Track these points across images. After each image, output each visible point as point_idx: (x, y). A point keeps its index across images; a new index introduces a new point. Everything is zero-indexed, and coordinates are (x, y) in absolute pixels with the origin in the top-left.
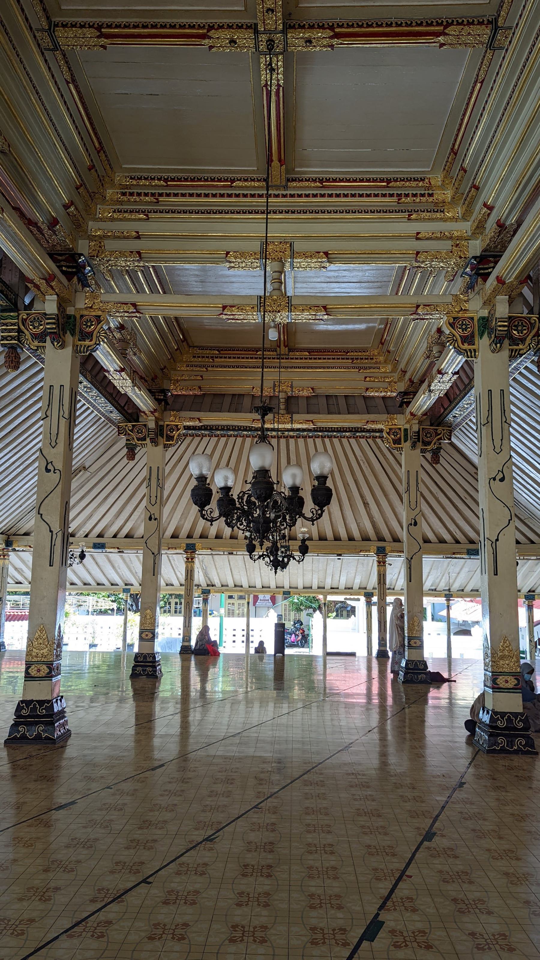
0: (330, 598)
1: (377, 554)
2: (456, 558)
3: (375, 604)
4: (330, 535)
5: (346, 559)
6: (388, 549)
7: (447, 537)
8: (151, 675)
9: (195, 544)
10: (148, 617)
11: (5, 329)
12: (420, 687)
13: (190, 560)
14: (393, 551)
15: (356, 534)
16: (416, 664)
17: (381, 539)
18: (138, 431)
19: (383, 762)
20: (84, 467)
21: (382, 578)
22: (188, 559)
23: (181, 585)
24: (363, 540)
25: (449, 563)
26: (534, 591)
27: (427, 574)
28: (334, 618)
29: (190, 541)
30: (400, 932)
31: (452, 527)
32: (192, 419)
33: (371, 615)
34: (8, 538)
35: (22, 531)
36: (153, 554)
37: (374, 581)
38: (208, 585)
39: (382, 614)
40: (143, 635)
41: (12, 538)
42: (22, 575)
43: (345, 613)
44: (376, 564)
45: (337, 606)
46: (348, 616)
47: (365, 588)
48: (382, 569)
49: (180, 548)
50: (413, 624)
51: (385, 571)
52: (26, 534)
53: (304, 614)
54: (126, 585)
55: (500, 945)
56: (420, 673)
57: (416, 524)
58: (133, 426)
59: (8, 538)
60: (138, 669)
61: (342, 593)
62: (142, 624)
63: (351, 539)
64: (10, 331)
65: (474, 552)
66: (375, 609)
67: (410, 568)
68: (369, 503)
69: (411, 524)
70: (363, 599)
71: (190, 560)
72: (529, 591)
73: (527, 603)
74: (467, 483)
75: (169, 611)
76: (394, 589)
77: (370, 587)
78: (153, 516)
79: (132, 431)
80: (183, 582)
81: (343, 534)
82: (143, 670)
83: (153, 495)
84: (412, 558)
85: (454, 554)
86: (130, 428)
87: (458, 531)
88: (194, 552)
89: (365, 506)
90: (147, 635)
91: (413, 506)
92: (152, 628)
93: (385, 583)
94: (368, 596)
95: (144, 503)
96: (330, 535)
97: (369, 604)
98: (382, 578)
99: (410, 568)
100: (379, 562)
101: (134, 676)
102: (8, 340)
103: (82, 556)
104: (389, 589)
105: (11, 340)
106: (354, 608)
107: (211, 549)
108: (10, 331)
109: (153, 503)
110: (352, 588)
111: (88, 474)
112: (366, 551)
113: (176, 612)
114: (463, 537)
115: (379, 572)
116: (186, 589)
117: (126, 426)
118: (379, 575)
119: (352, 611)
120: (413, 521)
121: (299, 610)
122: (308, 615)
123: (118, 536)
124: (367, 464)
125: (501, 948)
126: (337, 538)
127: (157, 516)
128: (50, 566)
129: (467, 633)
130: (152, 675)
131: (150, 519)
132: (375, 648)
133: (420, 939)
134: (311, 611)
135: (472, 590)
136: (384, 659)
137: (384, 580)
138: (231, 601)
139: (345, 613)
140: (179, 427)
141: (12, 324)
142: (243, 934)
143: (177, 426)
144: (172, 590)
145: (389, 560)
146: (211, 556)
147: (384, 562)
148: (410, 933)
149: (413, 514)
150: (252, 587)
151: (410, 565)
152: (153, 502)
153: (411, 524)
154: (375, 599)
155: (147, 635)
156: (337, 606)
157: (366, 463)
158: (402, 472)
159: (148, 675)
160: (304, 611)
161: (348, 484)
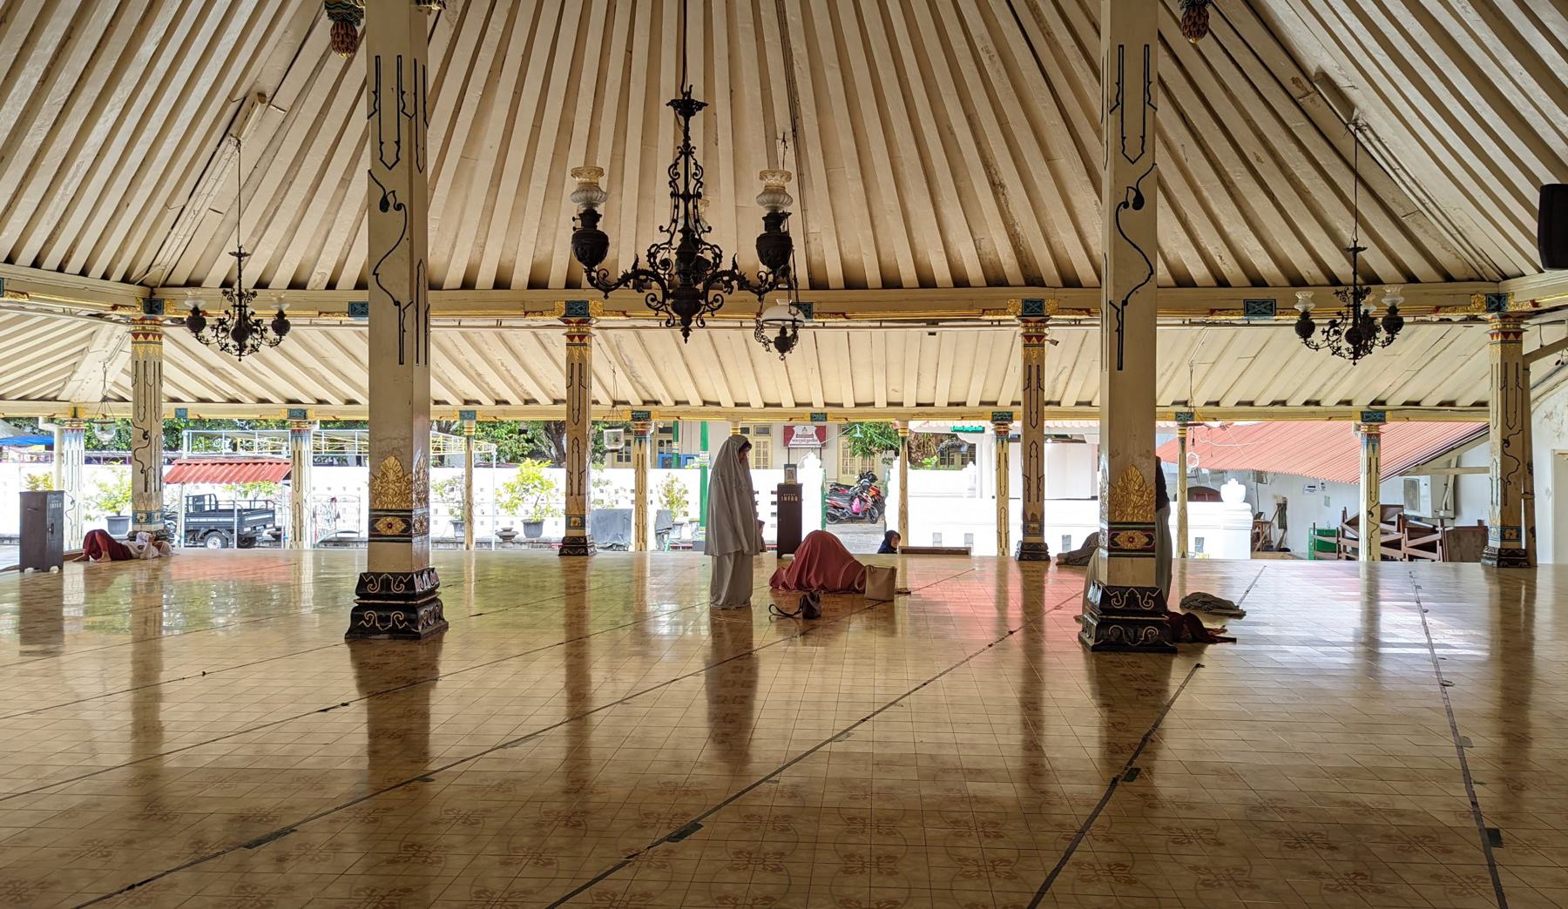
0: (914, 425)
1: (1024, 317)
2: (1214, 324)
3: (1016, 439)
4: (908, 274)
5: (947, 333)
6: (1049, 306)
7: (1198, 271)
8: (403, 631)
9: (586, 303)
10: (392, 477)
12: (1147, 662)
13: (578, 341)
14: (1062, 310)
15: (974, 271)
16: (1132, 599)
17: (1033, 279)
19: (1034, 765)
20: (261, 95)
21: (1033, 377)
22: (571, 337)
23: (556, 402)
24: (989, 284)
25: (1194, 340)
26: (1383, 403)
28: (936, 467)
29: (574, 295)
31: (1215, 247)
33: (1000, 540)
34: (152, 294)
35: (181, 276)
36: (397, 303)
37: (1010, 390)
38: (645, 403)
39: (1034, 460)
40: (380, 526)
41: (161, 293)
42: (232, 383)
43: (957, 458)
44: (1019, 342)
45: (942, 445)
46: (964, 463)
47: (995, 403)
48: (1035, 352)
49: (552, 311)
50: (1125, 488)
51: (1041, 357)
53: (878, 458)
54: (467, 402)
56: (1145, 624)
57: (1139, 202)
59: (152, 294)
60: (367, 614)
61: (942, 415)
62: (375, 495)
63: (960, 281)
65: (1262, 308)
66: (1015, 452)
67: (1120, 331)
68: (1006, 181)
69: (1126, 205)
70: (989, 426)
71: (578, 341)
72: (1372, 403)
73: (1364, 428)
74: (1267, 113)
76: (1059, 404)
77: (1004, 403)
78: (390, 198)
80: (563, 394)
81: (942, 273)
82: (381, 619)
83: (390, 138)
84: (1125, 303)
85: (1212, 312)
87: (1226, 253)
89: (995, 193)
90: (390, 526)
91: (1133, 151)
92: (404, 506)
93: (1040, 387)
94: (1001, 419)
95: (365, 163)
96: (908, 274)
97: (1002, 437)
98: (1033, 377)
99: (1120, 331)
100: (1027, 337)
101: (357, 634)
103: (281, 326)
104: (1048, 403)
106: (972, 447)
107: (624, 313)
109: (390, 160)
110: (964, 404)
111: (276, 116)
112: (997, 311)
114: (1238, 270)
115: (1027, 359)
116: (571, 409)
119: (970, 455)
120: (1132, 194)
121: (867, 453)
122: (884, 461)
124: (999, 65)
126: (926, 282)
127: (402, 198)
129: (1214, 496)
130: (406, 631)
131: (384, 205)
132: (1016, 536)
134: (891, 453)
135: (1238, 404)
136: (1038, 565)
137: (1040, 379)
139: (957, 458)
145: (1052, 332)
146: (631, 332)
147: (1041, 337)
149: (1132, 175)
150: (958, 404)
151: (1121, 323)
153: (1126, 205)
154: (1016, 427)
155: (390, 526)
156: (942, 445)
157: (997, 58)
158: (1103, 49)
159: (395, 633)
160: (878, 455)
161: (950, 128)
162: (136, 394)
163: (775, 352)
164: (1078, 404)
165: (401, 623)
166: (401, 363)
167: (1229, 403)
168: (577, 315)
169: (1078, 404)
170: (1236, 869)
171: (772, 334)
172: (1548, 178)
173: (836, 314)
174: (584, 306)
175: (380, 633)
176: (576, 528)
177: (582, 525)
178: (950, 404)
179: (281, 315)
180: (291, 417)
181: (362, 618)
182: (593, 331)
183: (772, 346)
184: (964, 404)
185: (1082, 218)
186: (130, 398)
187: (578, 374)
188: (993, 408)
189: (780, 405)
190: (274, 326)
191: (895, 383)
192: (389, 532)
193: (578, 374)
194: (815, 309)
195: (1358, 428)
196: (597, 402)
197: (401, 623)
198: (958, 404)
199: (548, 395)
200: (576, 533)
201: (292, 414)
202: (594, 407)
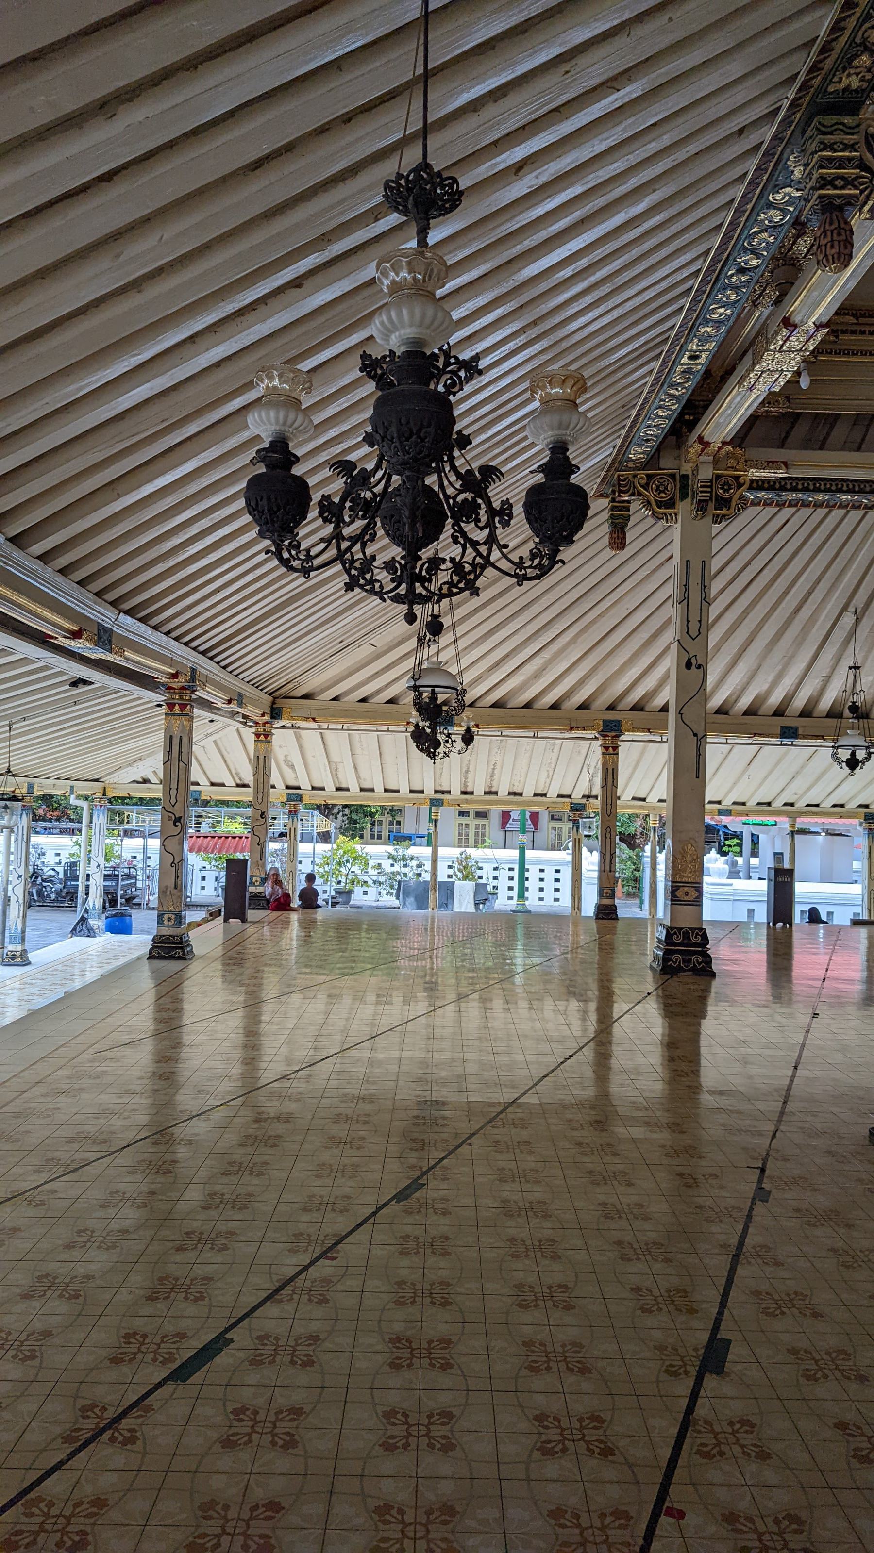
11: (830, 159)
18: (658, 487)
22: (258, 736)
27: (713, 771)
30: (555, 1419)
32: (772, 464)
36: (695, 735)
38: (436, 792)
41: (280, 703)
49: (592, 728)
52: (306, 697)
55: (742, 1446)
58: (648, 475)
60: (674, 957)
64: (842, 163)
71: (610, 751)
75: (379, 837)
78: (693, 661)
79: (646, 487)
86: (643, 482)
88: (619, 736)
90: (687, 894)
102: (836, 188)
105: (843, 188)
108: (842, 163)
109: (694, 632)
110: (521, 794)
113: (372, 837)
116: (256, 792)
117: (635, 476)
118: (605, 770)
123: (478, 704)
125: (744, 1453)
128: (697, 777)
131: (689, 665)
133: (592, 1435)
138: (464, 820)
140: (741, 480)
141: (846, 147)
142: (275, 1427)
143: (737, 478)
144: (347, 798)
148: (574, 1421)
150: (443, 792)
152: (694, 632)
162: (256, 781)
163: (847, 770)
164: (634, 799)
165: (699, 964)
166: (697, 777)
167: (778, 804)
168: (614, 731)
169: (535, 795)
170: (762, 1246)
171: (845, 754)
172: (253, 534)
173: (816, 737)
174: (618, 723)
175: (685, 971)
176: (607, 897)
177: (613, 896)
178: (535, 795)
179: (468, 730)
180: (288, 800)
181: (671, 960)
182: (273, 731)
183: (844, 764)
184: (545, 795)
185: (523, 630)
186: (251, 784)
187: (610, 775)
188: (717, 806)
189: (398, 791)
190: (463, 739)
191: (390, 770)
192: (686, 898)
193: (610, 775)
194: (800, 732)
195: (861, 824)
196: (273, 787)
197: (699, 964)
198: (443, 792)
199: (284, 780)
200: (607, 902)
201: (290, 798)
202: (272, 790)
